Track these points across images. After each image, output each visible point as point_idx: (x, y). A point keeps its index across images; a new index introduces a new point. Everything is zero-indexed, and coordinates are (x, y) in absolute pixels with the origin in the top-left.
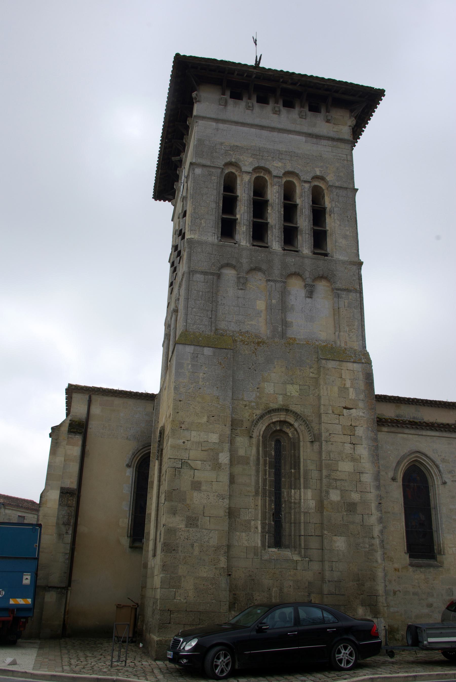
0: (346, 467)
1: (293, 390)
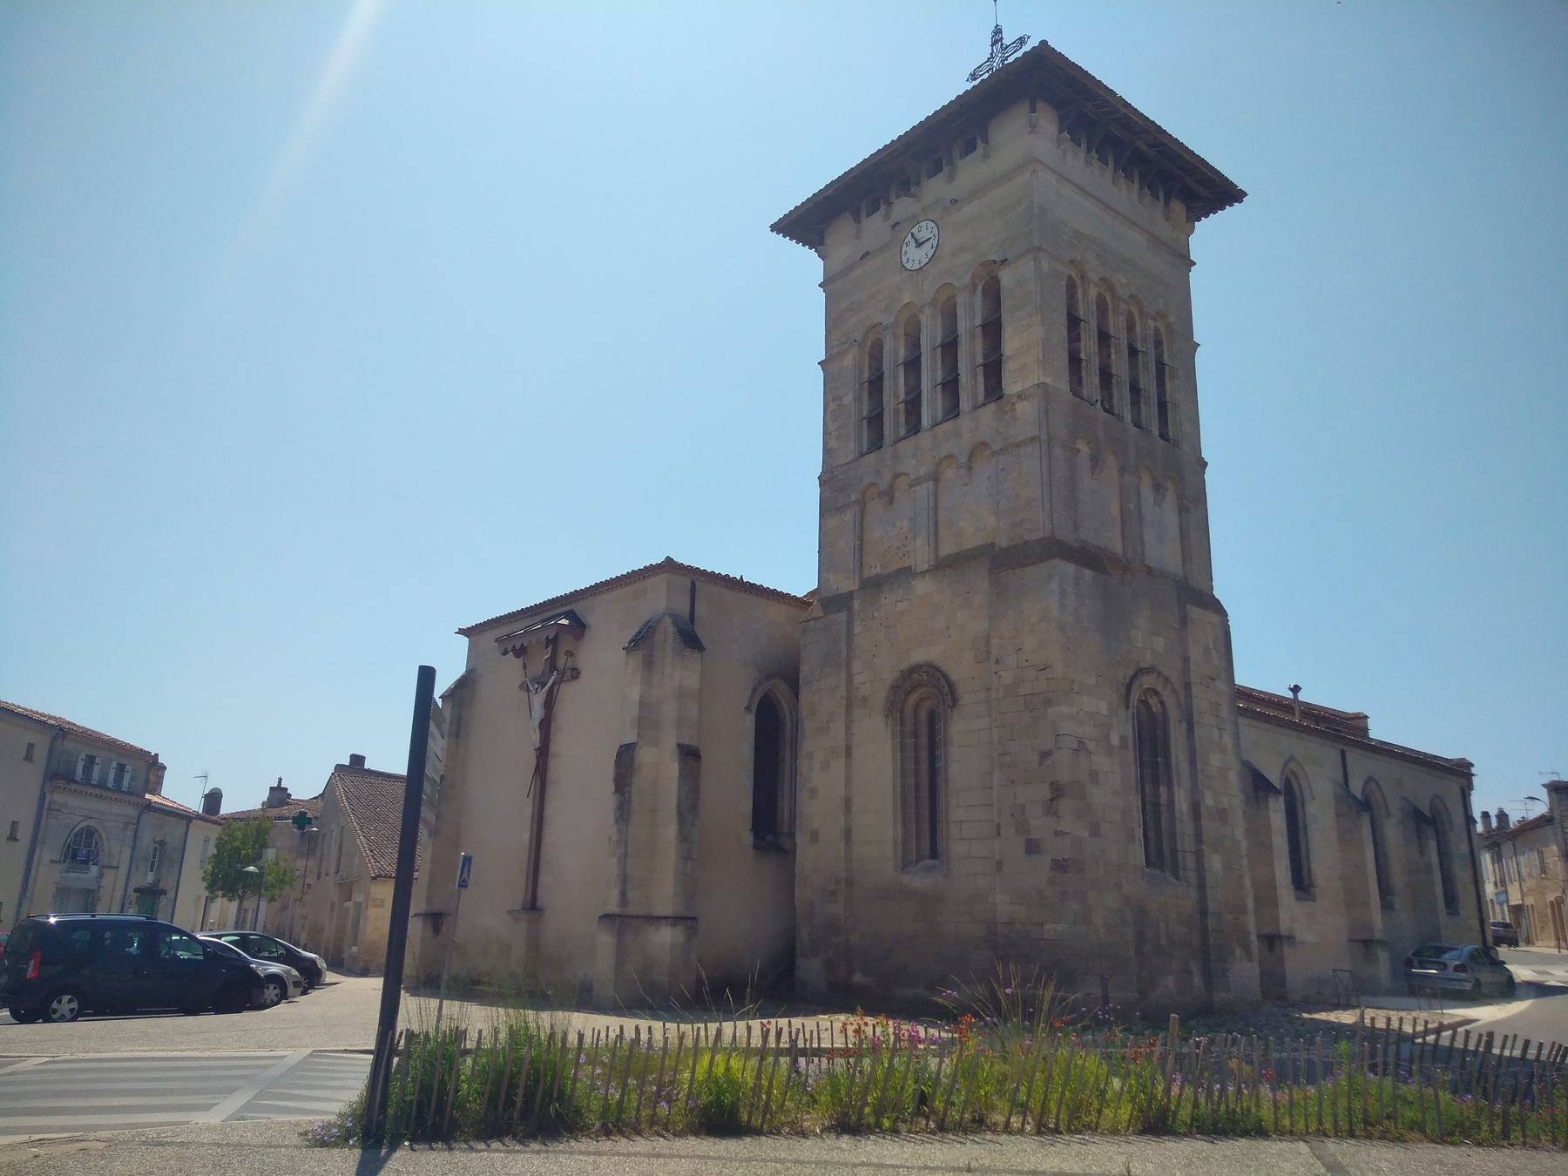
0: (1215, 759)
1: (1159, 643)
